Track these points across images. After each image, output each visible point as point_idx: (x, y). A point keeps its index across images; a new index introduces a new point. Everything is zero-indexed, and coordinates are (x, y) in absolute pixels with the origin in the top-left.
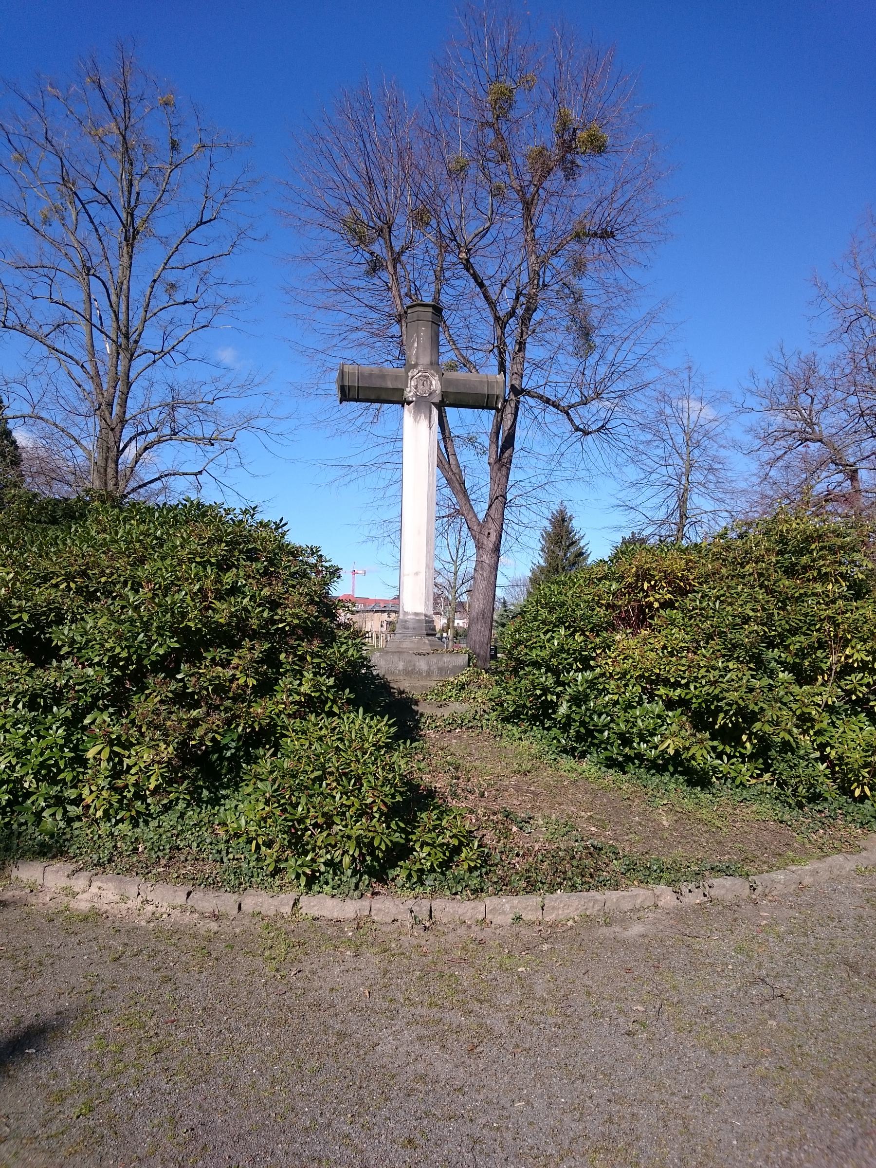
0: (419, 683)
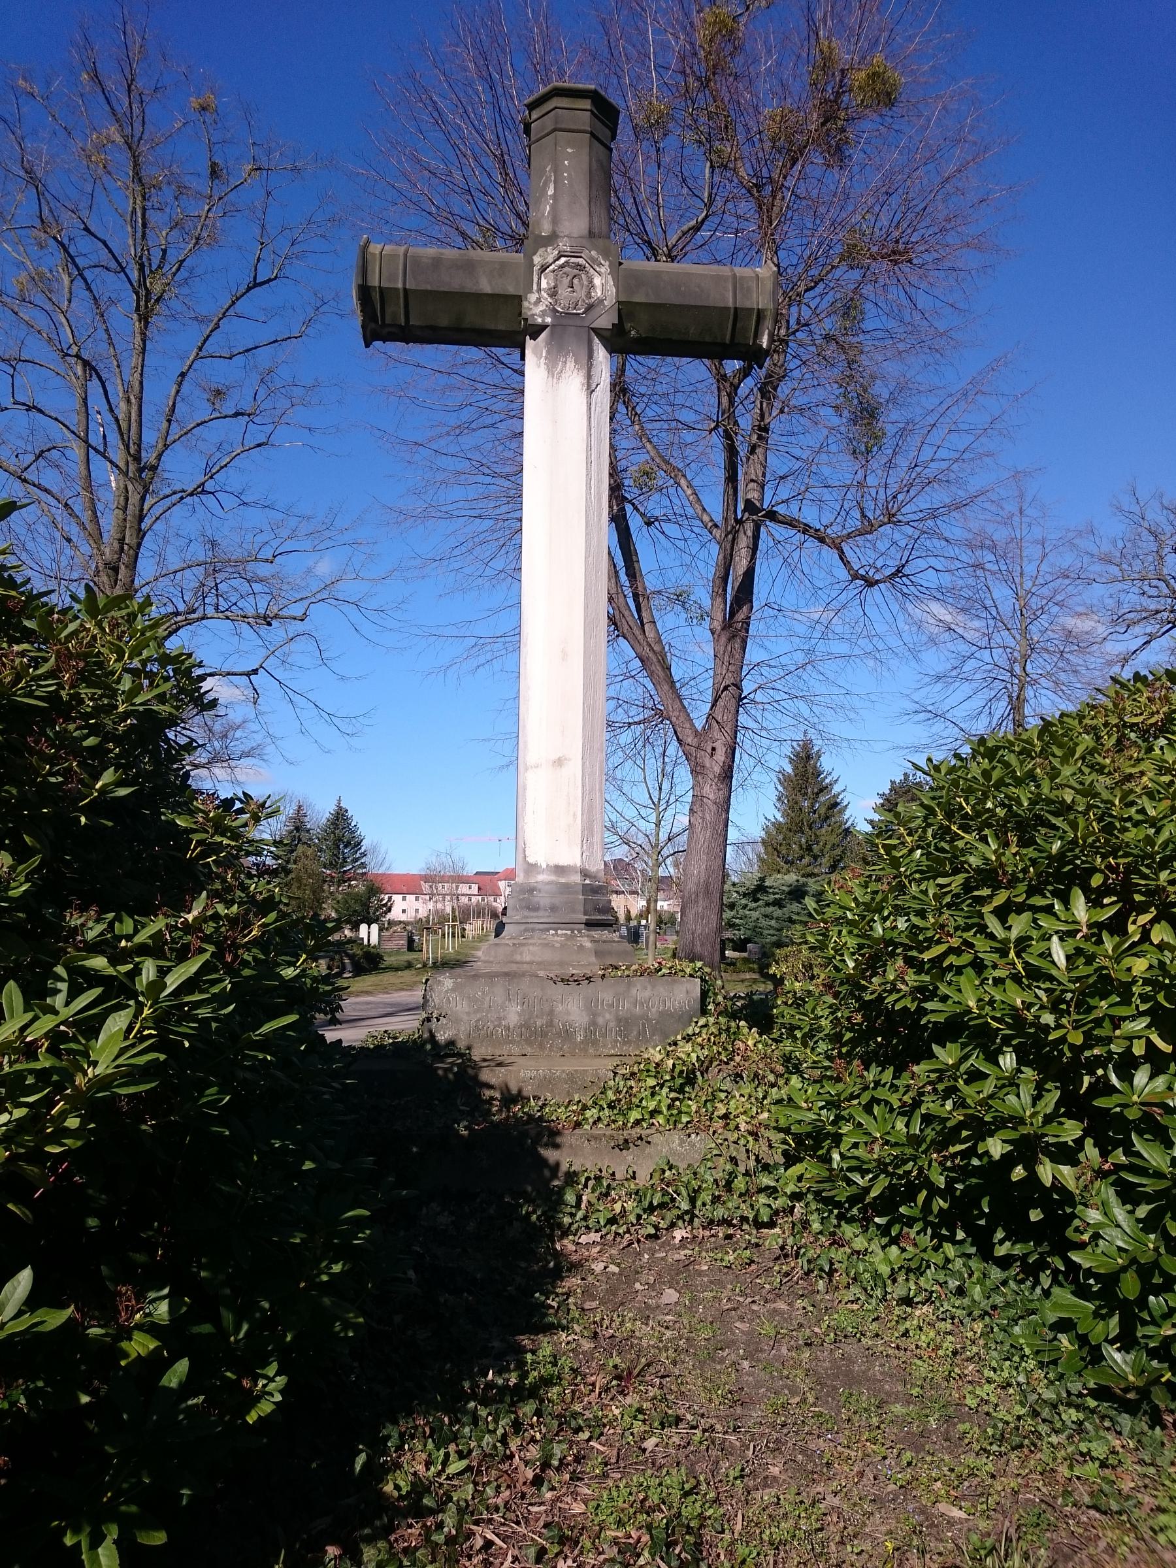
0: (563, 1067)
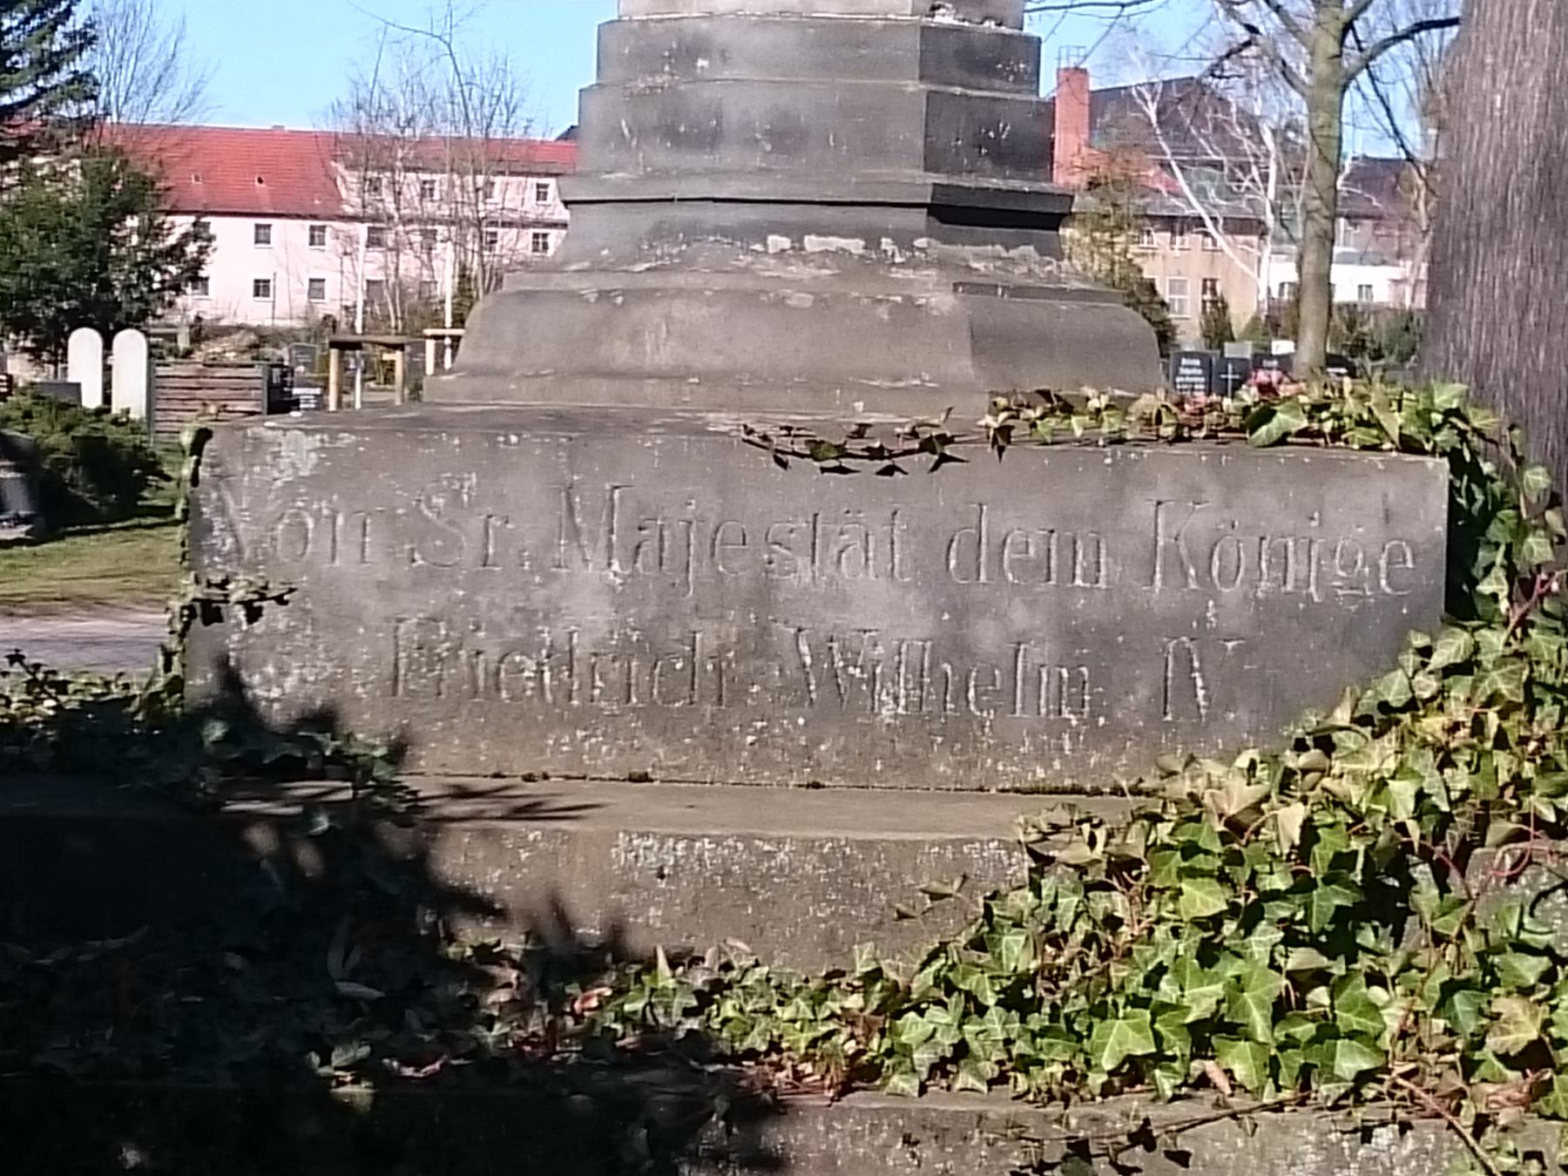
0: (801, 830)
